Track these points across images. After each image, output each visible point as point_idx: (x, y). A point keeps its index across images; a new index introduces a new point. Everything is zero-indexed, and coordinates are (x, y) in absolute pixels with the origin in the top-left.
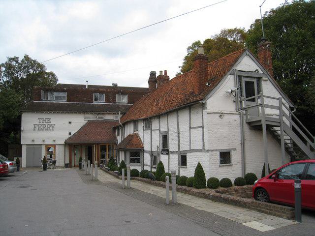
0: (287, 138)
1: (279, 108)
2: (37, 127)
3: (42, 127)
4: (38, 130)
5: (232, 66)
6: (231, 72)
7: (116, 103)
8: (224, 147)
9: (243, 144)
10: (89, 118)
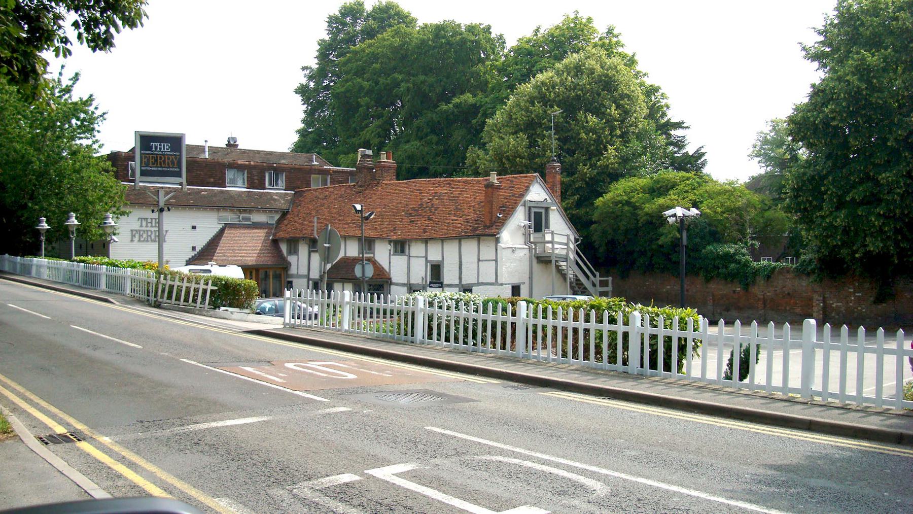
0: (572, 272)
1: (567, 244)
2: (137, 236)
3: (145, 236)
4: (139, 241)
5: (522, 196)
6: (522, 203)
7: (264, 188)
8: (515, 281)
9: (531, 278)
10: (226, 218)
